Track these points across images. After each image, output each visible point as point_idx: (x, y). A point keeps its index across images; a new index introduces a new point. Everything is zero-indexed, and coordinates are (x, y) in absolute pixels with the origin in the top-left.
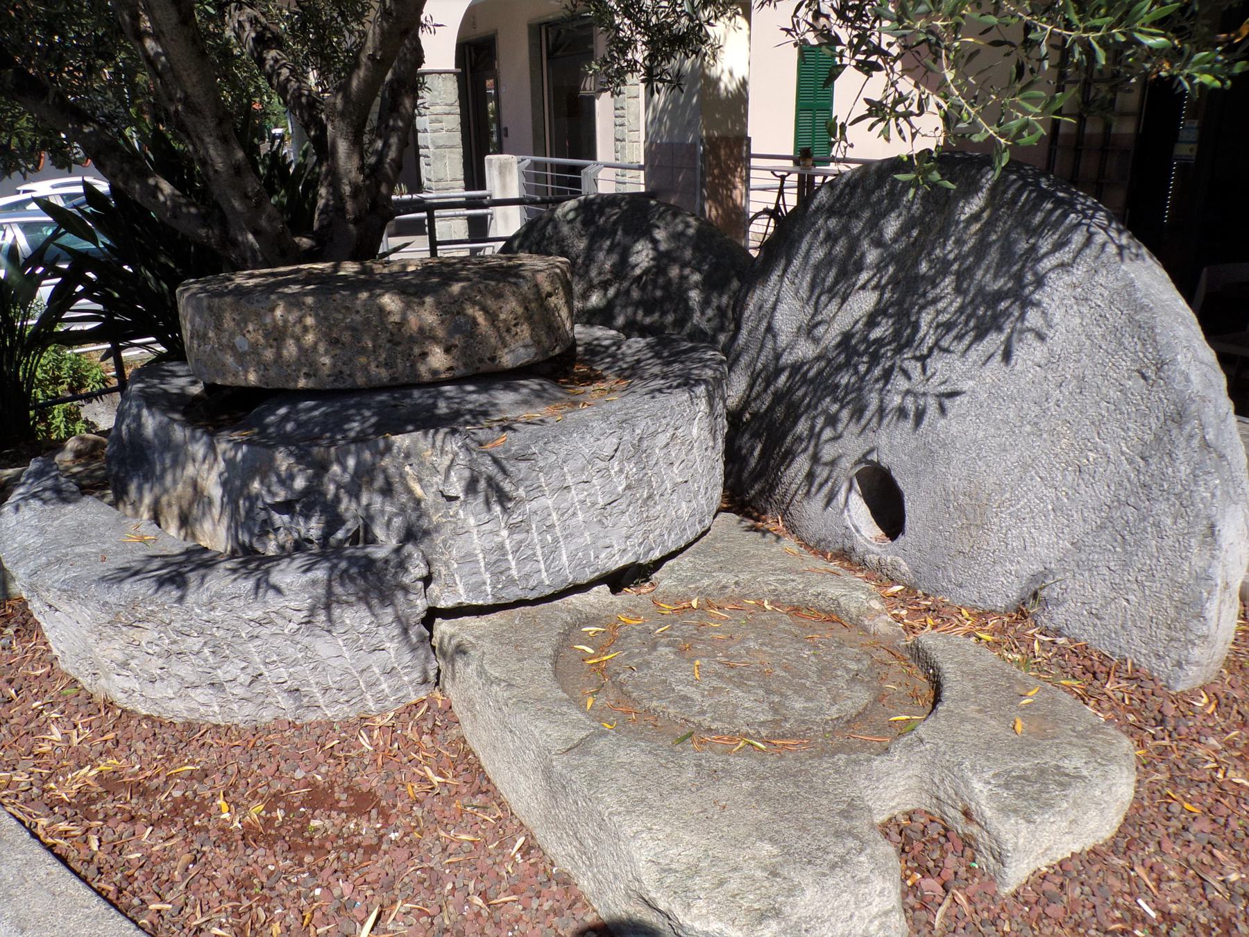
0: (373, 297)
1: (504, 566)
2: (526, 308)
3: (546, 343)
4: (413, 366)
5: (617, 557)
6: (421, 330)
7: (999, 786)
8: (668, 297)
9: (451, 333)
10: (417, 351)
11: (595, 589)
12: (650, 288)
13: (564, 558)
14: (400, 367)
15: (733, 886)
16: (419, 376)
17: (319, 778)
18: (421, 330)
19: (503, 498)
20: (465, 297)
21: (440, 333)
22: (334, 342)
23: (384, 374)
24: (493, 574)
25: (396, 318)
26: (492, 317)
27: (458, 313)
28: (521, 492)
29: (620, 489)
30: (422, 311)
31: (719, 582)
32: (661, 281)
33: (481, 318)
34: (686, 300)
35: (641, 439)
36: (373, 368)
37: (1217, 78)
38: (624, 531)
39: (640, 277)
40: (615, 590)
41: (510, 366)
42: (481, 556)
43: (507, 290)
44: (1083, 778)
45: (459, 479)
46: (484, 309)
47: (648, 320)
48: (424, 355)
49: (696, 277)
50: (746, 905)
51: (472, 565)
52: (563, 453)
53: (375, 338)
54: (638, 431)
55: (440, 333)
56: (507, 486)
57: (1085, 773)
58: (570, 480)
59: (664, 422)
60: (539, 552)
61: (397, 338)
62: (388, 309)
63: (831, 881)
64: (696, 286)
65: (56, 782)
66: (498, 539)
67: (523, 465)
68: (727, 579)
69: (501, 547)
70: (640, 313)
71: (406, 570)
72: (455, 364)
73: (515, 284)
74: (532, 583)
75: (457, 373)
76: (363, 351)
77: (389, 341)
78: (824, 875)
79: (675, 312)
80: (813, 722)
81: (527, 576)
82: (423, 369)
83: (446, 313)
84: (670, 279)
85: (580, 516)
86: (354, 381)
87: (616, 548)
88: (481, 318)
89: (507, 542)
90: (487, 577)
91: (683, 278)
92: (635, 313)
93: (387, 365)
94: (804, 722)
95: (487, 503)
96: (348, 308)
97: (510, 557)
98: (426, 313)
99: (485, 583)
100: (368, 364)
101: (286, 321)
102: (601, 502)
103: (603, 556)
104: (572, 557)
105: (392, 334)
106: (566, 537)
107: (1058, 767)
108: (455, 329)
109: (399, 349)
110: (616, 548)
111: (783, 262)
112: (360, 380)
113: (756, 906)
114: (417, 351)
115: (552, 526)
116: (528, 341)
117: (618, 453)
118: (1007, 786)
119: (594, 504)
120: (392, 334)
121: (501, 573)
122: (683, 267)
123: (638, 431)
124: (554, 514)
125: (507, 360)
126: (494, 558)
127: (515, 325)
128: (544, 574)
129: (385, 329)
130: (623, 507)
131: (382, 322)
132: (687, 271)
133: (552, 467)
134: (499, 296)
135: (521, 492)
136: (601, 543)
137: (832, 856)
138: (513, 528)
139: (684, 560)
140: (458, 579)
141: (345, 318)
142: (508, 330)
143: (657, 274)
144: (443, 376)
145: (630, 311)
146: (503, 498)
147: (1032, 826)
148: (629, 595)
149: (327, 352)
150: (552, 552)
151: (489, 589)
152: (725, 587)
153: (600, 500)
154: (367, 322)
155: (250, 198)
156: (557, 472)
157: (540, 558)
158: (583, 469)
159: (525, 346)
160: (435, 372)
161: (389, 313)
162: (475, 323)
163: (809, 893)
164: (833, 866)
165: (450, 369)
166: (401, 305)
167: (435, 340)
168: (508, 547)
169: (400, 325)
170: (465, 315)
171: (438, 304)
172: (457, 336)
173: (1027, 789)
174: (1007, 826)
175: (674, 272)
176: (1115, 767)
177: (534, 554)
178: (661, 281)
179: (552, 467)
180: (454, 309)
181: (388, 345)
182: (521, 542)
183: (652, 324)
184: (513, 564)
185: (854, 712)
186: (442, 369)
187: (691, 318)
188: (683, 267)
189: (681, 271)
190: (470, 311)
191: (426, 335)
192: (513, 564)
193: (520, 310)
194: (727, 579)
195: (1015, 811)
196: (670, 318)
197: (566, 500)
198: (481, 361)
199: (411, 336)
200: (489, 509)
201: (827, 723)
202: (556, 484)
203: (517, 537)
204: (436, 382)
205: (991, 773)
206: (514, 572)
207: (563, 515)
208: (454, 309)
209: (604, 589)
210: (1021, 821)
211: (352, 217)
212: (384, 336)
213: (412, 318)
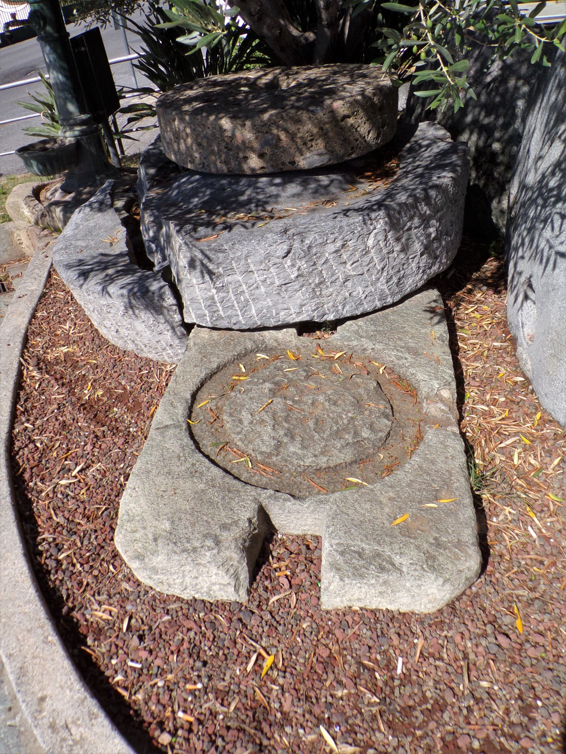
0: (218, 119)
1: (215, 309)
2: (321, 129)
3: (340, 151)
4: (240, 164)
5: (294, 316)
6: (244, 142)
7: (337, 551)
8: (502, 104)
9: (263, 146)
10: (241, 155)
11: (285, 330)
12: (493, 93)
13: (253, 311)
14: (233, 164)
15: (138, 535)
16: (244, 171)
17: (128, 388)
18: (244, 142)
19: (211, 273)
20: (272, 122)
21: (256, 145)
22: (199, 145)
23: (225, 168)
24: (210, 312)
25: (229, 134)
26: (292, 136)
27: (267, 132)
28: (221, 270)
29: (293, 276)
30: (243, 130)
31: (362, 345)
32: (501, 89)
33: (283, 136)
34: (514, 107)
35: (310, 247)
36: (219, 164)
37: (494, 80)
38: (299, 301)
39: (489, 83)
40: (300, 334)
41: (307, 167)
42: (202, 301)
43: (304, 116)
44: (401, 572)
45: (185, 257)
46: (286, 131)
47: (486, 121)
48: (246, 158)
49: (526, 89)
50: (136, 547)
51: (197, 304)
52: (245, 252)
53: (219, 145)
54: (307, 242)
55: (256, 145)
56: (211, 267)
57: (405, 569)
58: (252, 268)
59: (332, 236)
60: (236, 305)
61: (229, 146)
62: (224, 127)
63: (176, 557)
64: (523, 97)
65: (52, 350)
66: (210, 294)
67: (220, 255)
68: (368, 345)
69: (212, 298)
70: (483, 114)
71: (164, 300)
72: (265, 165)
73: (312, 112)
74: (234, 321)
75: (266, 170)
76: (213, 152)
77: (226, 148)
78: (175, 553)
79: (505, 117)
80: (291, 463)
81: (229, 317)
82: (245, 167)
83: (259, 132)
84: (507, 88)
85: (263, 289)
86: (210, 170)
87: (293, 311)
88: (283, 136)
89: (216, 296)
90: (206, 312)
91: (516, 88)
92: (479, 114)
93: (226, 162)
94: (286, 461)
95: (202, 272)
96: (204, 125)
97: (218, 305)
98: (246, 132)
99: (206, 315)
100: (216, 161)
101: (179, 129)
102: (277, 283)
103: (282, 313)
104: (259, 311)
105: (227, 144)
106: (253, 300)
107: (390, 557)
108: (266, 143)
109: (231, 153)
110: (293, 311)
111: (541, 96)
112: (213, 170)
113: (139, 550)
114: (241, 155)
115: (243, 292)
116: (323, 150)
117: (290, 255)
118: (342, 553)
119: (272, 283)
120: (227, 144)
121: (214, 312)
122: (519, 78)
123: (307, 242)
124: (244, 286)
125: (303, 162)
126: (208, 303)
127: (311, 140)
128: (241, 318)
129: (223, 140)
130: (297, 287)
131: (222, 136)
132: (521, 83)
133: (239, 259)
134: (298, 121)
135: (221, 270)
136: (280, 306)
137: (189, 545)
138: (218, 290)
139: (360, 322)
140: (191, 310)
141: (203, 131)
142: (305, 144)
143: (500, 82)
144: (259, 172)
145: (477, 110)
146: (211, 273)
147: (341, 583)
148: (306, 339)
149: (197, 151)
150: (245, 306)
151: (208, 319)
152: (365, 350)
153: (276, 281)
154: (214, 135)
155: (253, 16)
156: (243, 262)
157: (237, 308)
158: (261, 262)
159: (320, 155)
160: (253, 170)
161: (225, 130)
162: (279, 139)
163: (160, 558)
164: (184, 551)
165: (263, 168)
166: (231, 125)
167: (252, 149)
168: (216, 299)
169: (233, 136)
170: (271, 134)
171: (254, 126)
172: (266, 148)
173: (354, 561)
174: (328, 575)
175: (512, 83)
176: (433, 577)
177: (233, 306)
178: (501, 89)
179: (239, 259)
180: (264, 129)
181: (225, 150)
182: (224, 298)
183: (488, 124)
184: (220, 308)
185: (324, 465)
186: (257, 167)
187: (514, 123)
188: (519, 78)
189: (516, 82)
190: (275, 131)
191: (246, 146)
192: (220, 308)
193: (315, 131)
194: (368, 345)
195: (338, 570)
196: (501, 121)
197: (252, 278)
198: (283, 164)
199: (238, 146)
200: (203, 277)
201: (299, 466)
202: (243, 269)
203: (222, 294)
204: (255, 175)
205: (337, 541)
206: (221, 313)
207: (250, 287)
208: (264, 129)
209: (294, 331)
210: (337, 577)
211: (326, 23)
212: (224, 144)
213: (238, 134)
